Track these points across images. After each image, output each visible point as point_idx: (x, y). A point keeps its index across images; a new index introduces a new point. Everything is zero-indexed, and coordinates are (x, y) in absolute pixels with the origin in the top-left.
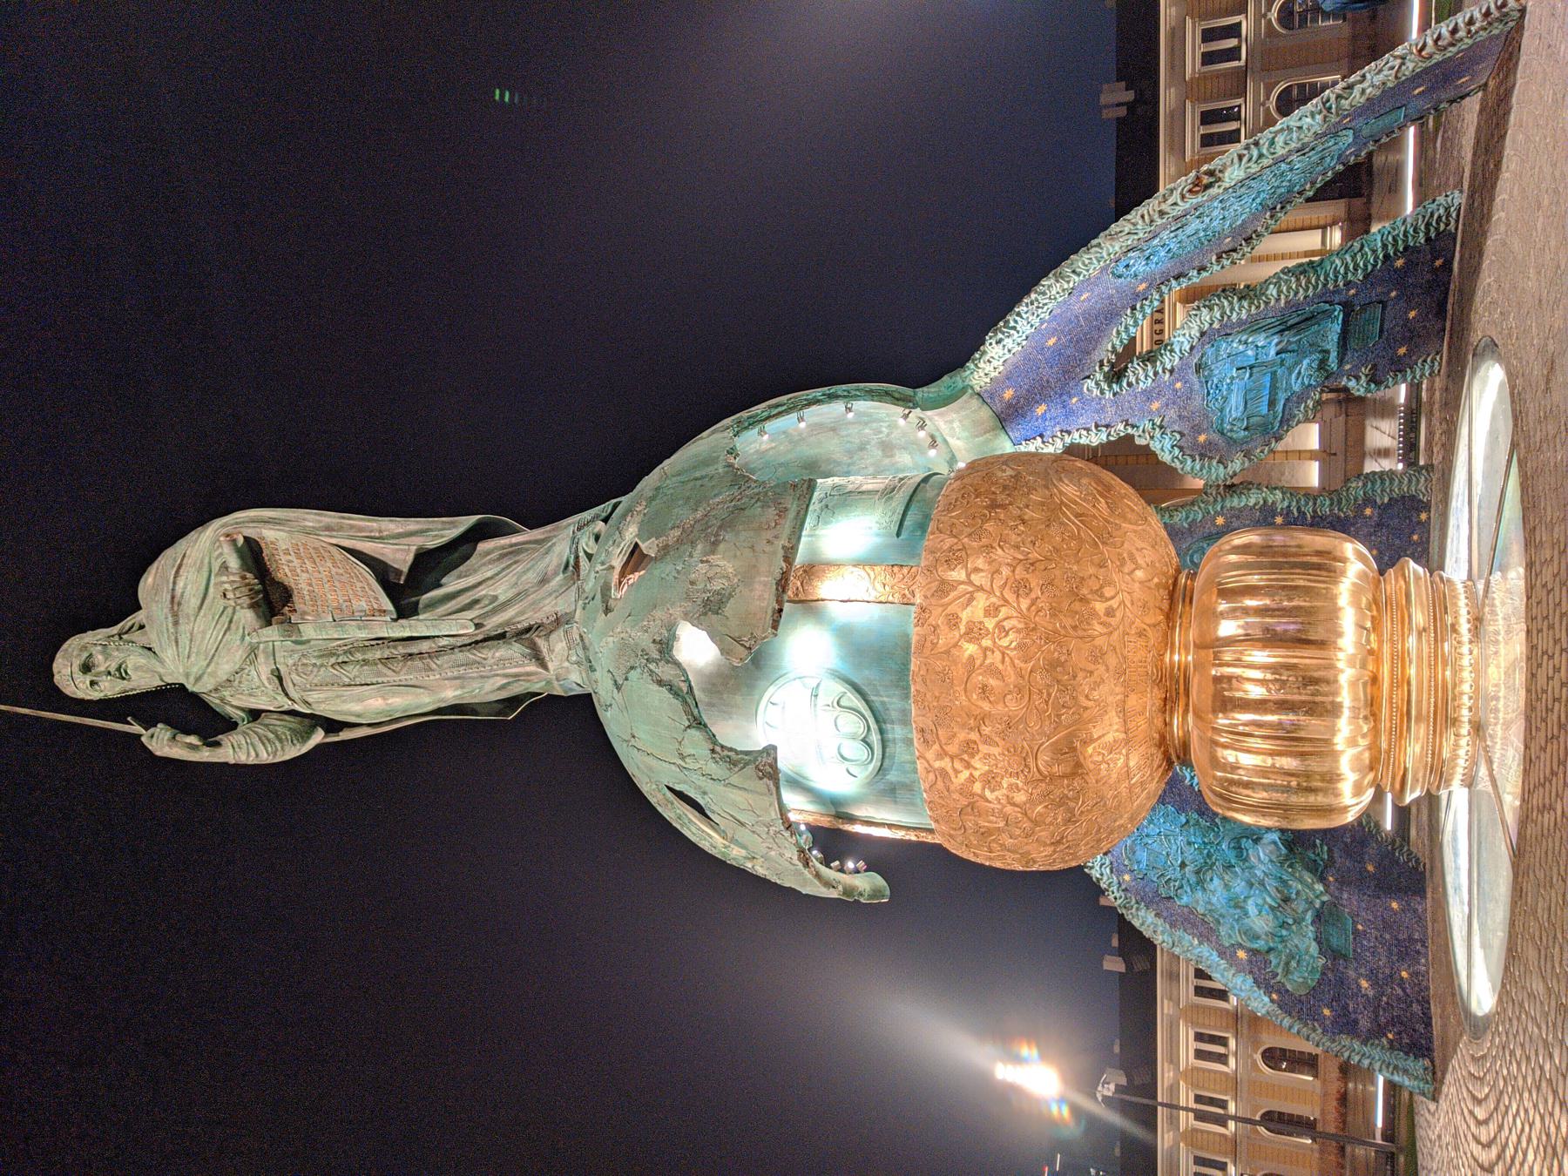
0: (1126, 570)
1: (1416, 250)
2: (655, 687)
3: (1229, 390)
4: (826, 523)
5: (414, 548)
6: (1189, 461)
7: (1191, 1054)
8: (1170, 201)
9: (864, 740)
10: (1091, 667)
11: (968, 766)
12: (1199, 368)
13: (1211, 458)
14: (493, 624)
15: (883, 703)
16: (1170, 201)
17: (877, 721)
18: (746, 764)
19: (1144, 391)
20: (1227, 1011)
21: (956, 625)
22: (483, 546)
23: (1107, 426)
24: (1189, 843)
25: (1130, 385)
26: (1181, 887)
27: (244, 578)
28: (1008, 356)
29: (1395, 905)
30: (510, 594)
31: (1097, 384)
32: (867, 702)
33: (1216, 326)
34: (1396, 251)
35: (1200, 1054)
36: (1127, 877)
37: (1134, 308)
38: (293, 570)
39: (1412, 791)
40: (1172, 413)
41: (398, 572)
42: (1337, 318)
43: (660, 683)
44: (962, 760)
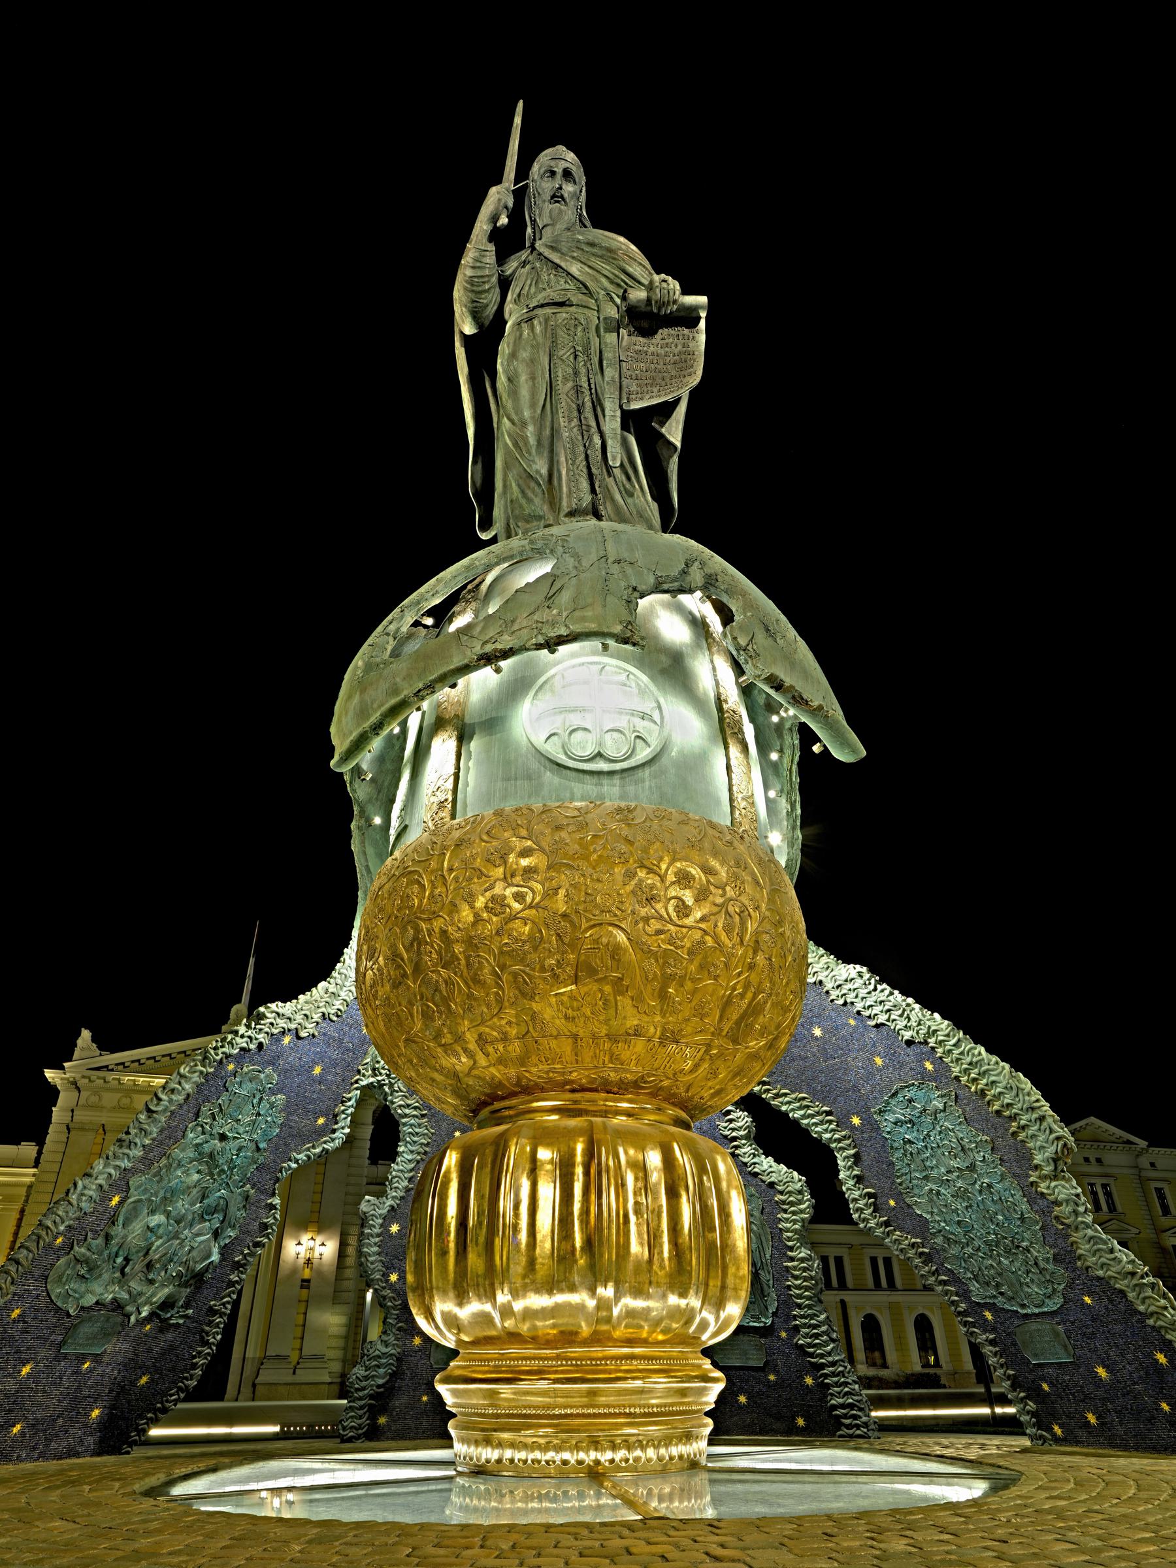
1: (823, 1398)
9: (599, 755)
15: (643, 781)
17: (623, 771)
24: (239, 1150)
29: (96, 1413)
32: (643, 765)
33: (778, 1197)
34: (826, 1376)
36: (231, 1067)
39: (455, 1393)
41: (662, 424)
42: (758, 1320)
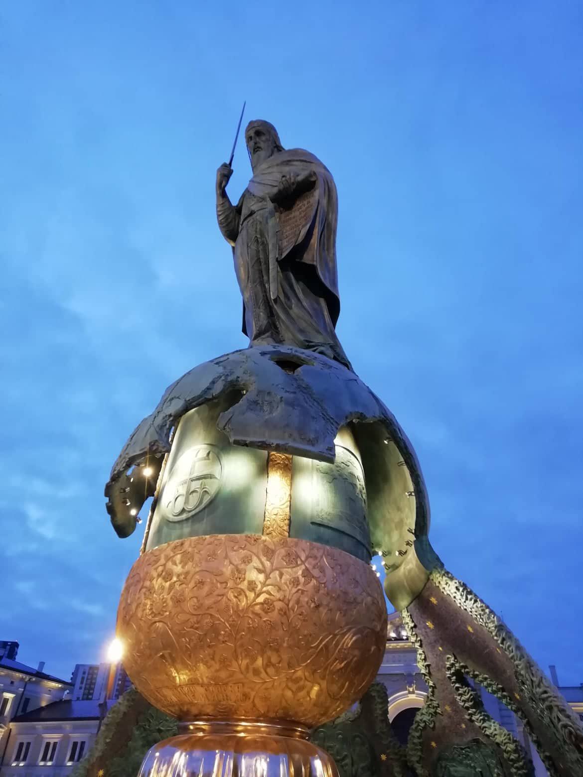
0: (290, 684)
2: (210, 380)
3: (468, 766)
4: (323, 478)
5: (315, 263)
6: (417, 734)
7: (48, 741)
8: (560, 716)
10: (217, 658)
11: (159, 576)
12: (477, 741)
13: (422, 750)
14: (277, 308)
16: (560, 716)
17: (193, 516)
18: (160, 435)
19: (455, 699)
20: (37, 760)
21: (244, 562)
22: (322, 302)
23: (429, 673)
25: (457, 689)
26: (145, 730)
27: (293, 184)
28: (452, 596)
30: (293, 315)
31: (453, 665)
35: (75, 744)
37: (503, 690)
38: (301, 208)
40: (445, 721)
43: (213, 382)
44: (163, 571)
